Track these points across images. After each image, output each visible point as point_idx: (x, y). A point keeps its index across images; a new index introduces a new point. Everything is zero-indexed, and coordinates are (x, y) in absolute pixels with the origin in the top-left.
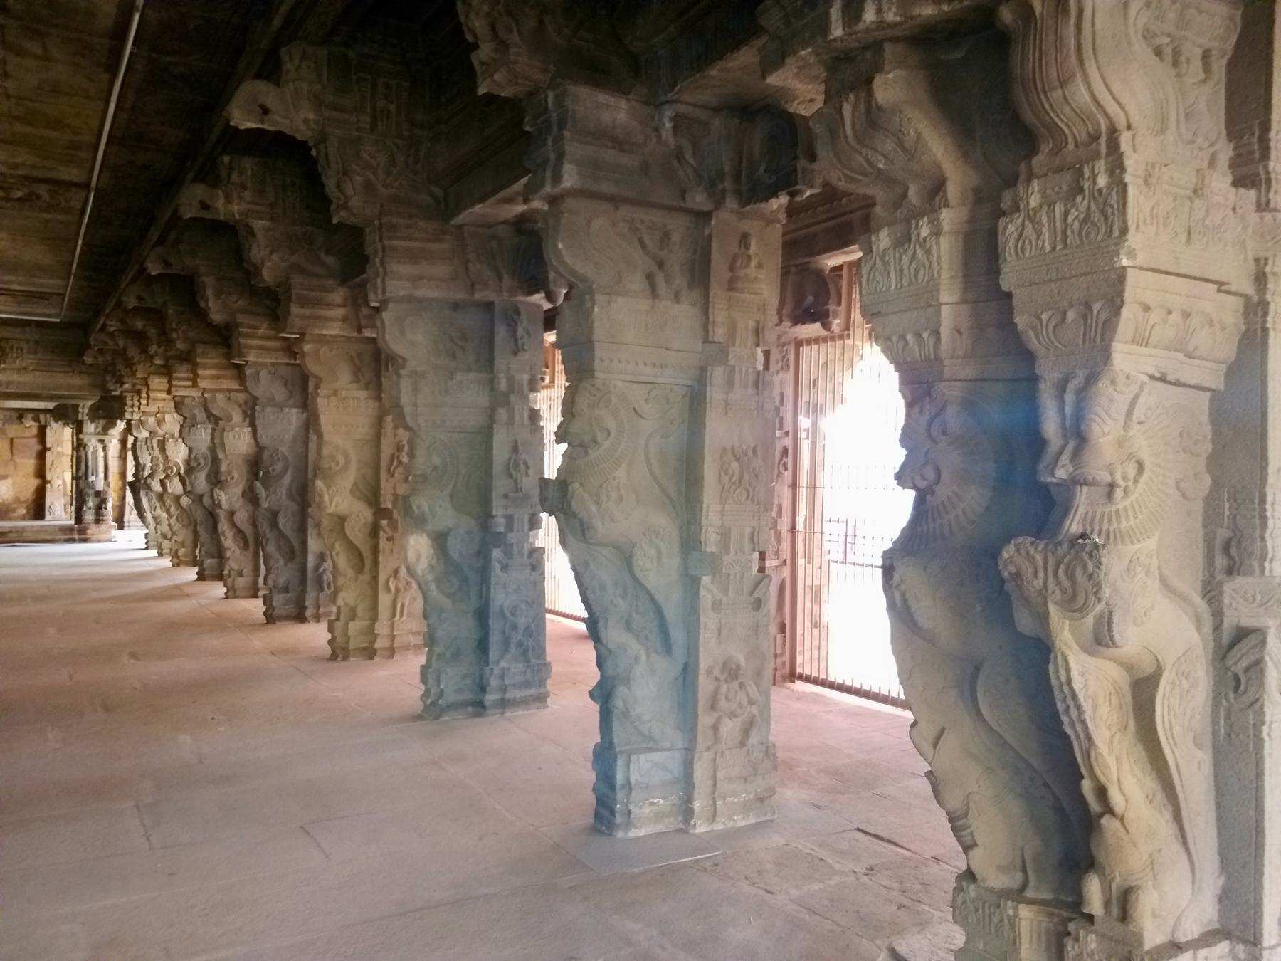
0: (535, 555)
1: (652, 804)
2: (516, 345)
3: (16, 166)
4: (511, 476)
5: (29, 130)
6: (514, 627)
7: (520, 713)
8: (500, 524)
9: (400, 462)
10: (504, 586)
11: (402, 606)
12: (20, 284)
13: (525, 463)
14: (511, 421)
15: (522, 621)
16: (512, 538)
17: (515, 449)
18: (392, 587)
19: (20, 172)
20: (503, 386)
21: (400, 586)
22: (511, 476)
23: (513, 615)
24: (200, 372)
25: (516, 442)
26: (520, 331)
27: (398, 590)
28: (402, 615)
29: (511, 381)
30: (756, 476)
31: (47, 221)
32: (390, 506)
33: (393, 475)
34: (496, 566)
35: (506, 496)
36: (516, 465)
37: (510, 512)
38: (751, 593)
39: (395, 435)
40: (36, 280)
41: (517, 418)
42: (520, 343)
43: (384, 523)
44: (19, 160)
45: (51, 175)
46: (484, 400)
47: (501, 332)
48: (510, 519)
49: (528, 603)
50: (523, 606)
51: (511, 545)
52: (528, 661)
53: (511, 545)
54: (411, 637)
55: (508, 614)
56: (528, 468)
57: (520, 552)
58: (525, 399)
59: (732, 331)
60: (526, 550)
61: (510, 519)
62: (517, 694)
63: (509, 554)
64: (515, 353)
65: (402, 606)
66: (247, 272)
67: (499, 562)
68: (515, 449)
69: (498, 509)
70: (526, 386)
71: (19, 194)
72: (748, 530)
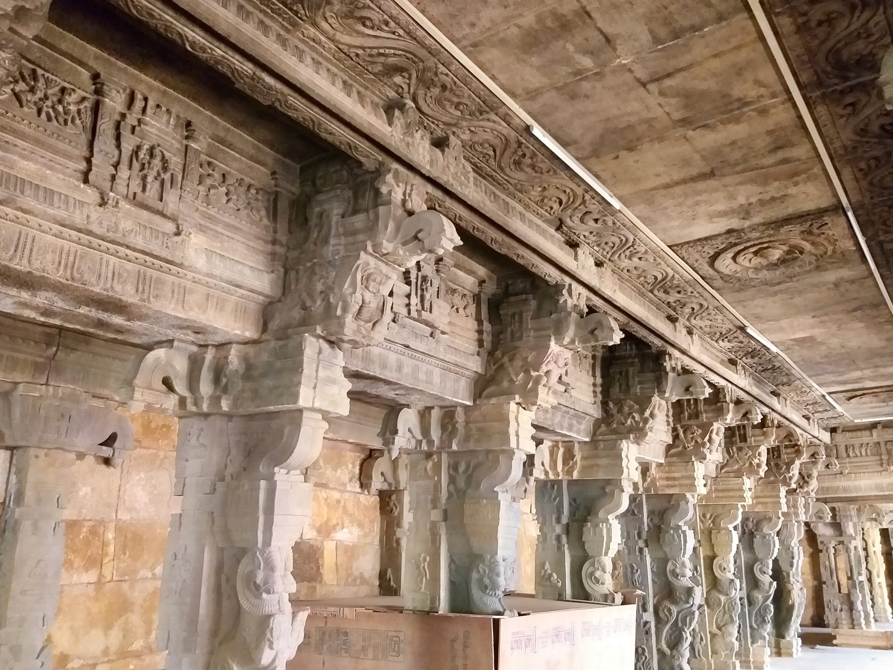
3: (745, 212)
5: (707, 140)
12: (872, 379)
19: (757, 219)
31: (837, 285)
40: (883, 371)
44: (742, 200)
45: (791, 208)
71: (776, 254)
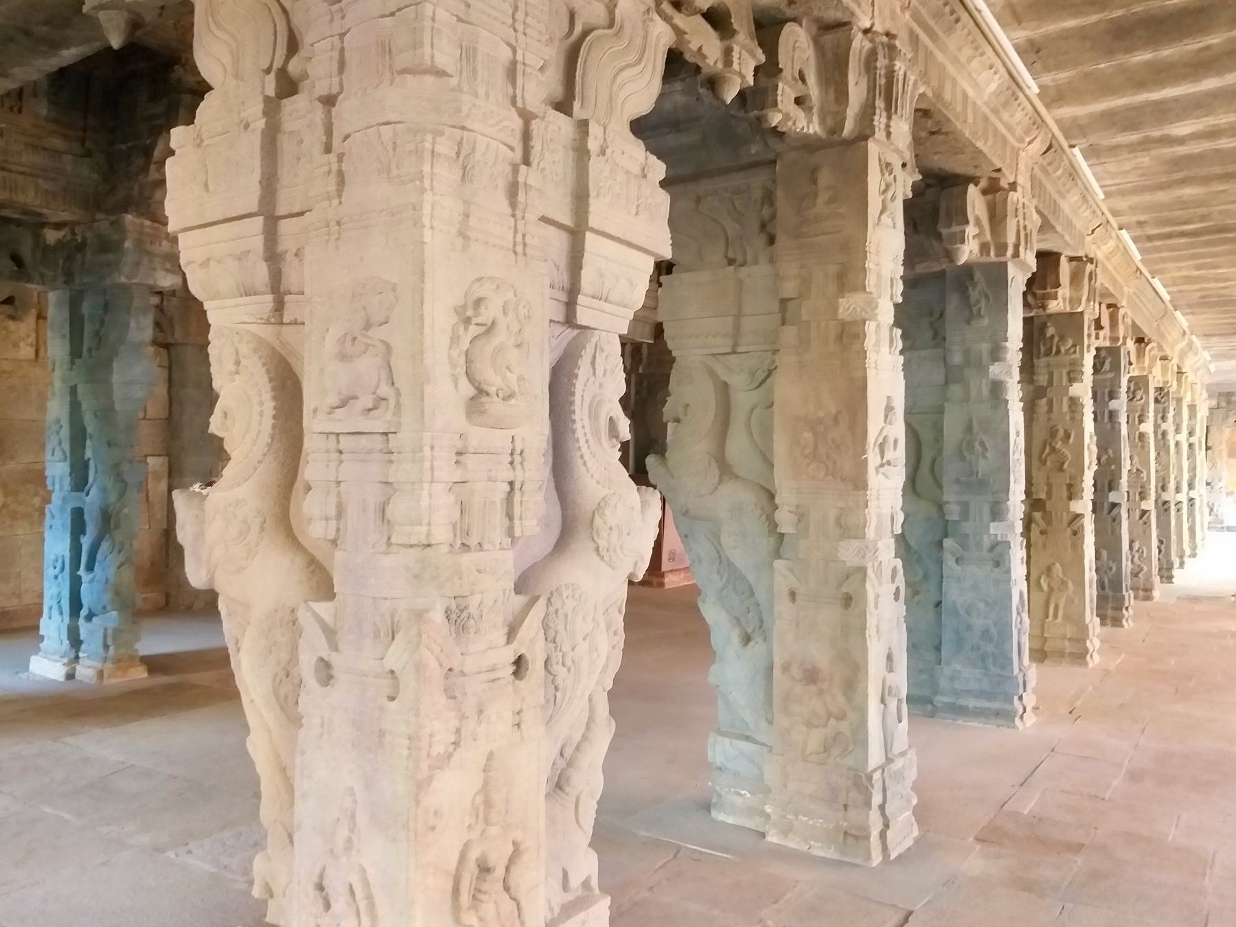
0: (998, 549)
1: (739, 794)
2: (971, 312)
4: (963, 458)
6: (969, 628)
7: (975, 724)
8: (953, 512)
9: (1053, 449)
10: (958, 580)
11: (1056, 608)
13: (982, 444)
14: (966, 399)
15: (978, 622)
16: (967, 527)
17: (969, 429)
18: (1045, 587)
20: (957, 359)
21: (1055, 585)
22: (963, 458)
23: (968, 613)
24: (81, 655)
25: (971, 420)
26: (974, 294)
27: (1051, 589)
28: (1056, 616)
29: (967, 353)
30: (838, 447)
32: (1043, 496)
33: (1044, 463)
34: (949, 562)
35: (957, 481)
36: (970, 445)
37: (964, 498)
38: (840, 585)
39: (1049, 419)
41: (973, 394)
42: (975, 309)
43: (1037, 515)
46: (938, 376)
47: (953, 302)
48: (965, 506)
49: (987, 603)
50: (982, 606)
51: (968, 535)
52: (986, 668)
53: (968, 535)
54: (1067, 643)
55: (962, 612)
56: (985, 449)
57: (979, 545)
58: (983, 370)
59: (806, 283)
60: (986, 542)
61: (965, 506)
62: (971, 703)
63: (964, 546)
64: (968, 322)
65: (1056, 608)
66: (777, 275)
67: (952, 553)
68: (969, 429)
69: (951, 496)
70: (986, 358)
72: (833, 513)
